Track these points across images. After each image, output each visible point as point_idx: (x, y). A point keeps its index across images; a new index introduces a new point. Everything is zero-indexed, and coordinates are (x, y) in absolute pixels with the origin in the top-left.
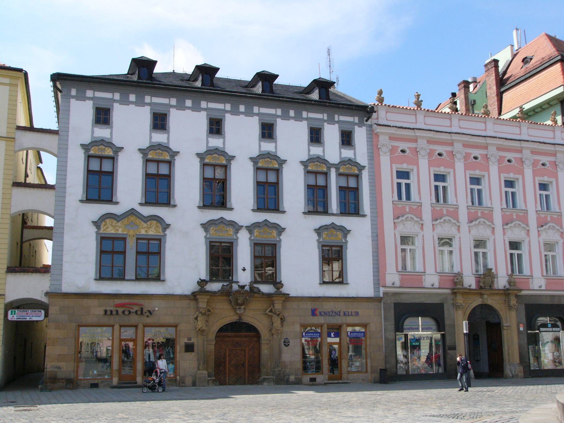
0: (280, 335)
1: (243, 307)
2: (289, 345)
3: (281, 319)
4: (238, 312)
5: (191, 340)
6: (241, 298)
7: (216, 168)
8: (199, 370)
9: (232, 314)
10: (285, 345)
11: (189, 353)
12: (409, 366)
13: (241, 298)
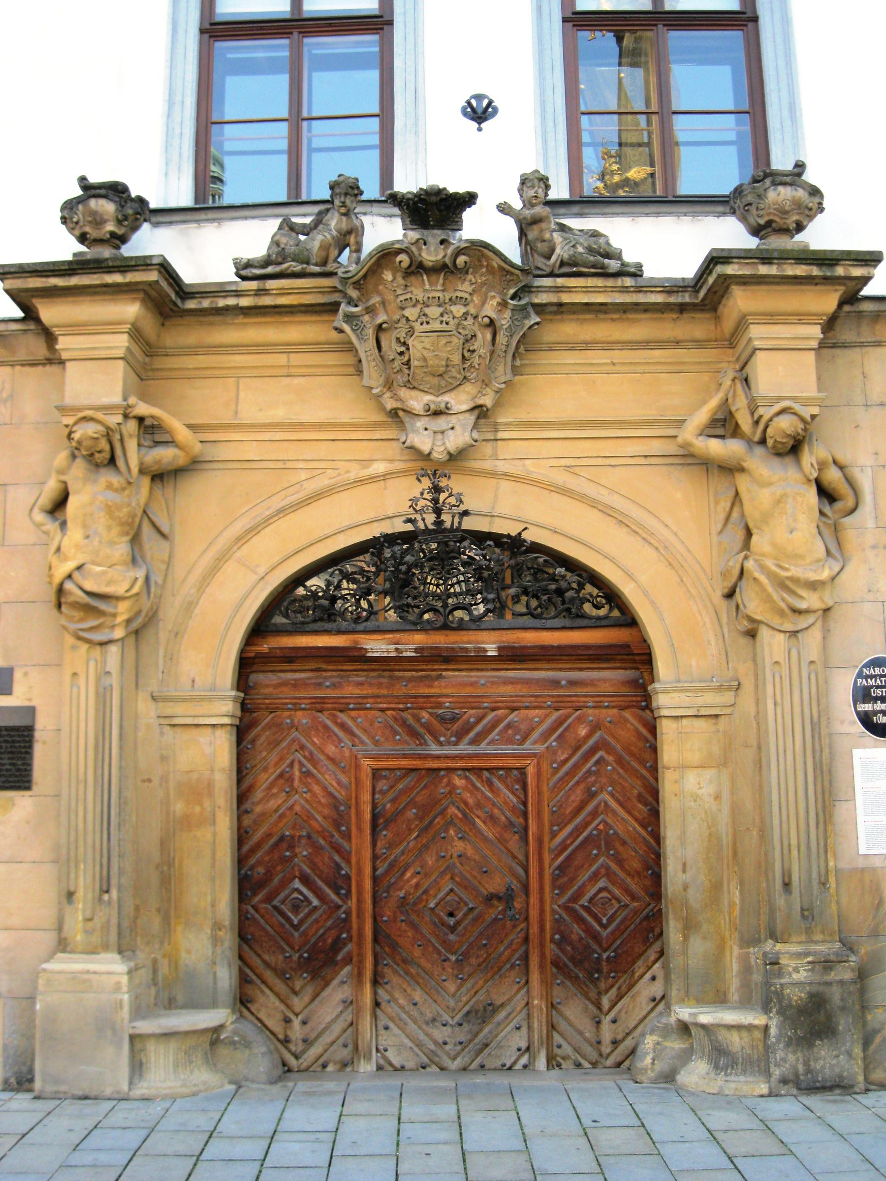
3: (826, 494)
4: (423, 442)
6: (434, 311)
8: (63, 945)
9: (380, 467)
10: (867, 721)
12: (481, 1030)
13: (434, 311)
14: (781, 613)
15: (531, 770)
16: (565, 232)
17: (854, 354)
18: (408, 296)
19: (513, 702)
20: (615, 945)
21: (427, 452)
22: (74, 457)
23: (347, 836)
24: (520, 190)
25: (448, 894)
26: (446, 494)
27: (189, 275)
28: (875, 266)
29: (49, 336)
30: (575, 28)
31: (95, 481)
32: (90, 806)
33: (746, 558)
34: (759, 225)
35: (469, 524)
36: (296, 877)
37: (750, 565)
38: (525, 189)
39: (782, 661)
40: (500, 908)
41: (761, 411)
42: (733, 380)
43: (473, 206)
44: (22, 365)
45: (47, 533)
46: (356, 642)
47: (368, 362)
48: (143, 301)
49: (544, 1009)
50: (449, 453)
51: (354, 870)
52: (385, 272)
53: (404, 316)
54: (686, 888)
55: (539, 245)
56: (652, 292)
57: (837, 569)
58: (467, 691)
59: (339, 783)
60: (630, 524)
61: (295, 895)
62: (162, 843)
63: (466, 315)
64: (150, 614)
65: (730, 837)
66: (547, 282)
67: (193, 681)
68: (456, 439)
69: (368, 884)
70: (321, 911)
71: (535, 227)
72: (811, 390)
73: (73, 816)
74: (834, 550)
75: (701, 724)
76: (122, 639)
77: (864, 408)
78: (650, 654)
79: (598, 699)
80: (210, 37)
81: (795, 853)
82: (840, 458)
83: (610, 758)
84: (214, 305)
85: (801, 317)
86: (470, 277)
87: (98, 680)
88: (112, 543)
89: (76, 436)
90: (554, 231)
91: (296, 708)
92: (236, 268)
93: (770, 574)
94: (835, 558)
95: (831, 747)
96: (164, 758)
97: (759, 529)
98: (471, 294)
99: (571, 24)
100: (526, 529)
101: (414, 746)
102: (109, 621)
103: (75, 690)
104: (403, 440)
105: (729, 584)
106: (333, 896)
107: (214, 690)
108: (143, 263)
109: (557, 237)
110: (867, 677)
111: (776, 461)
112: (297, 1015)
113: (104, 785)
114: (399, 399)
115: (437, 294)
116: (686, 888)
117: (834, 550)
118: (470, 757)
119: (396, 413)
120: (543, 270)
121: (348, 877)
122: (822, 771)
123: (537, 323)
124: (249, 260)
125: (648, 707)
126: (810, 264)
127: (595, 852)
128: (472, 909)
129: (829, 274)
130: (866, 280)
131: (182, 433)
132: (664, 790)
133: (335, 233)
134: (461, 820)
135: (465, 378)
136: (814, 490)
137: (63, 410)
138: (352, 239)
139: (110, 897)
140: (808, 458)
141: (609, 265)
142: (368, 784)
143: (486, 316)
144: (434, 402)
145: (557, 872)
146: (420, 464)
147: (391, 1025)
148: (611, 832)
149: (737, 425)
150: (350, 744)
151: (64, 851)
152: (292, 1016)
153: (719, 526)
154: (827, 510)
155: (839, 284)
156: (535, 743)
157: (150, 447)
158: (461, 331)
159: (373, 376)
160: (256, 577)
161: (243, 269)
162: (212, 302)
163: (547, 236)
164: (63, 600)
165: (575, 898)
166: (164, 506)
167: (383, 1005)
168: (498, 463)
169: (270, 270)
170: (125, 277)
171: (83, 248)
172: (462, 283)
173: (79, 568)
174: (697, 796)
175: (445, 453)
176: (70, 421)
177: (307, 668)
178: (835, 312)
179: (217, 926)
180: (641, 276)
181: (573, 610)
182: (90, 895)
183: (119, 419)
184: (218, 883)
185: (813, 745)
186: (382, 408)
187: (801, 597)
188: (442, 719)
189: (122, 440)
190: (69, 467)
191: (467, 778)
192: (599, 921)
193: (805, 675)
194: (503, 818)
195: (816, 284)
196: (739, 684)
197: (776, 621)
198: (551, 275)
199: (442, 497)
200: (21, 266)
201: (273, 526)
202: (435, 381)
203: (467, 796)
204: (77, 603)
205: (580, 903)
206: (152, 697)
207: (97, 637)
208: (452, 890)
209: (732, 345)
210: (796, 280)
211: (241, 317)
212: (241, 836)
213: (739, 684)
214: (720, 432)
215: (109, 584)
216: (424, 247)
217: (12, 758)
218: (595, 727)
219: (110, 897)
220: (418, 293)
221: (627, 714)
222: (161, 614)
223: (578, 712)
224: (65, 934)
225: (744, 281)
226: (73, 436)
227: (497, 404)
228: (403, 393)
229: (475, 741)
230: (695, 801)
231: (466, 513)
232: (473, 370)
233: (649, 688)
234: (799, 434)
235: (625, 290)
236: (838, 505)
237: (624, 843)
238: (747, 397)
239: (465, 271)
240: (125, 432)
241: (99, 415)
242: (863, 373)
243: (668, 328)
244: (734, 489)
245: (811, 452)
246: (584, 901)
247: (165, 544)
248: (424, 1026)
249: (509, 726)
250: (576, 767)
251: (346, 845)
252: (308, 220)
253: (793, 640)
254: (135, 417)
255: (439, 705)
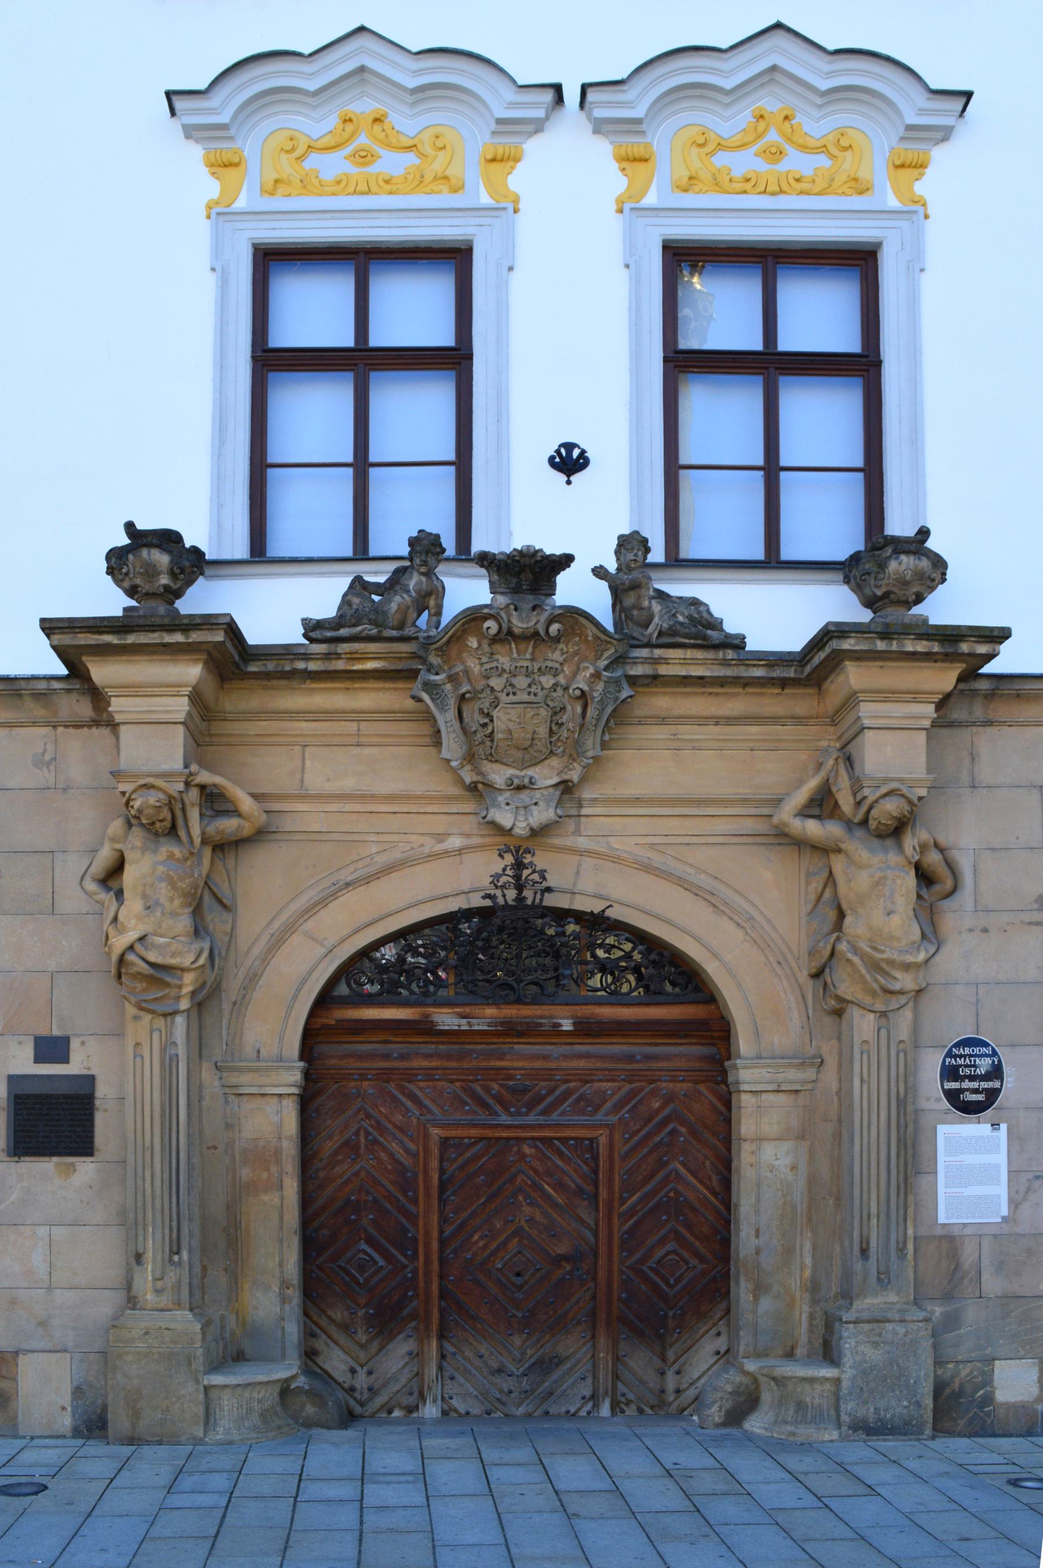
0: (908, 1014)
1: (546, 775)
2: (992, 1095)
3: (925, 877)
4: (504, 818)
5: (65, 1059)
6: (521, 682)
7: (683, 460)
9: (455, 842)
10: (952, 1096)
11: (48, 1166)
13: (521, 682)
14: (874, 994)
15: (603, 1140)
16: (664, 600)
17: (964, 735)
18: (494, 664)
19: (586, 1075)
20: (681, 1304)
21: (509, 827)
22: (130, 825)
23: (415, 1201)
24: (617, 553)
25: (515, 1255)
26: (529, 871)
27: (253, 636)
28: (1001, 643)
29: (97, 696)
30: (677, 369)
31: (155, 851)
32: (158, 1173)
33: (838, 939)
34: (875, 595)
35: (550, 901)
36: (361, 1239)
37: (843, 946)
38: (623, 551)
39: (871, 1041)
40: (568, 1269)
41: (866, 792)
42: (836, 760)
43: (567, 570)
44: (66, 727)
45: (101, 903)
46: (428, 1016)
47: (448, 733)
48: (206, 663)
49: (610, 1362)
50: (532, 829)
51: (421, 1232)
52: (470, 639)
53: (489, 686)
54: (758, 1252)
55: (635, 612)
56: (754, 665)
57: (932, 951)
58: (538, 1064)
59: (407, 1151)
60: (717, 904)
61: (361, 1256)
62: (228, 1207)
63: (556, 685)
64: (214, 986)
65: (805, 1206)
66: (644, 653)
67: (258, 1052)
68: (542, 814)
69: (435, 1246)
70: (385, 1272)
71: (632, 593)
72: (920, 771)
73: (140, 1182)
74: (928, 931)
75: (782, 1098)
76: (188, 1010)
77: (971, 790)
78: (729, 1031)
79: (673, 1073)
80: (264, 365)
81: (874, 1221)
82: (942, 840)
83: (683, 1130)
84: (280, 669)
85: (914, 696)
86: (561, 646)
87: (163, 1050)
88: (174, 914)
89: (137, 804)
90: (653, 598)
91: (363, 1077)
92: (305, 628)
93: (863, 956)
94: (931, 942)
95: (916, 1121)
96: (228, 1126)
97: (854, 910)
98: (561, 664)
99: (672, 364)
100: (610, 906)
101: (484, 1117)
102: (174, 992)
103: (138, 1060)
104: (484, 814)
105: (816, 965)
106: (402, 1259)
107: (281, 1061)
108: (208, 622)
109: (656, 607)
110: (955, 1056)
111: (876, 843)
112: (362, 1366)
113: (171, 1150)
114: (480, 773)
115: (525, 664)
116: (758, 1252)
117: (928, 931)
118: (541, 1127)
119: (476, 787)
120: (638, 640)
121: (415, 1240)
122: (905, 1146)
123: (631, 697)
124: (318, 621)
125: (725, 1081)
126: (933, 640)
127: (664, 1218)
128: (538, 1270)
129: (950, 650)
130: (990, 657)
131: (246, 803)
132: (739, 1161)
133: (414, 594)
134: (530, 1186)
135: (551, 752)
136: (913, 873)
137: (116, 774)
138: (432, 603)
139: (180, 1259)
140: (910, 842)
141: (711, 637)
142: (436, 1152)
143: (578, 688)
144: (518, 777)
145: (626, 1236)
146: (499, 839)
147: (457, 1375)
148: (682, 1199)
149: (836, 802)
150: (417, 1113)
151: (131, 1215)
152: (358, 1369)
153: (809, 907)
154: (924, 892)
155: (960, 661)
156: (607, 1114)
157: (212, 817)
158: (550, 703)
159: (452, 746)
160: (324, 951)
161: (312, 628)
162: (277, 665)
163: (646, 603)
164: (123, 970)
165: (643, 1260)
166: (225, 878)
167: (449, 1358)
168: (581, 839)
169: (343, 632)
170: (187, 637)
171: (133, 603)
172: (553, 653)
173: (142, 939)
174: (773, 1166)
175: (528, 829)
176: (127, 787)
177: (374, 1039)
178: (952, 691)
179: (285, 1284)
180: (743, 648)
181: (652, 987)
182: (159, 1257)
183: (181, 786)
184: (285, 1245)
185: (898, 1120)
186: (461, 781)
187: (895, 978)
188: (513, 1091)
189: (184, 810)
190: (126, 836)
191: (536, 1147)
192: (666, 1281)
193: (893, 1053)
194: (573, 1185)
195: (936, 661)
196: (822, 1062)
197: (868, 1001)
198: (648, 645)
199: (526, 873)
200: (70, 620)
201: (341, 899)
202: (519, 754)
203: (536, 1164)
204: (139, 973)
205: (648, 1264)
206: (216, 1067)
207: (160, 1008)
208: (519, 1252)
209: (834, 723)
210: (913, 656)
211: (308, 681)
212: (306, 1200)
213: (822, 1062)
214: (816, 811)
215: (173, 955)
216: (514, 613)
217: (72, 1126)
218: (669, 1099)
219: (180, 1259)
220: (504, 661)
221: (702, 1088)
222: (224, 985)
223: (652, 1086)
224: (133, 1293)
225: (858, 656)
226: (131, 803)
227: (583, 779)
228: (487, 767)
229: (545, 1112)
230: (771, 1171)
231: (549, 890)
232: (559, 744)
233: (727, 1063)
234: (905, 816)
235: (725, 663)
236: (937, 888)
237: (694, 1210)
238: (850, 779)
239: (557, 640)
240: (187, 801)
241: (160, 783)
242: (972, 754)
243: (772, 703)
244: (828, 869)
245: (914, 835)
246: (652, 1263)
247: (227, 917)
248: (490, 1377)
249: (580, 1098)
250: (649, 1136)
251: (412, 1208)
252: (382, 579)
253: (883, 1020)
254: (196, 785)
255: (511, 1077)
